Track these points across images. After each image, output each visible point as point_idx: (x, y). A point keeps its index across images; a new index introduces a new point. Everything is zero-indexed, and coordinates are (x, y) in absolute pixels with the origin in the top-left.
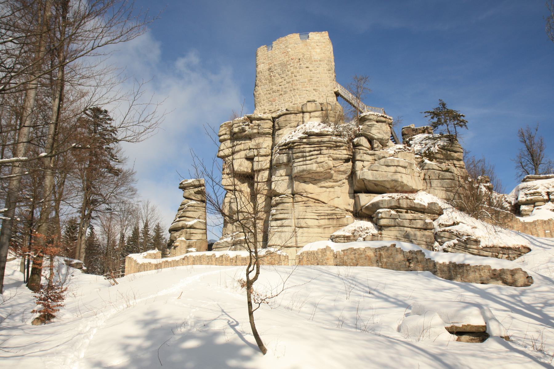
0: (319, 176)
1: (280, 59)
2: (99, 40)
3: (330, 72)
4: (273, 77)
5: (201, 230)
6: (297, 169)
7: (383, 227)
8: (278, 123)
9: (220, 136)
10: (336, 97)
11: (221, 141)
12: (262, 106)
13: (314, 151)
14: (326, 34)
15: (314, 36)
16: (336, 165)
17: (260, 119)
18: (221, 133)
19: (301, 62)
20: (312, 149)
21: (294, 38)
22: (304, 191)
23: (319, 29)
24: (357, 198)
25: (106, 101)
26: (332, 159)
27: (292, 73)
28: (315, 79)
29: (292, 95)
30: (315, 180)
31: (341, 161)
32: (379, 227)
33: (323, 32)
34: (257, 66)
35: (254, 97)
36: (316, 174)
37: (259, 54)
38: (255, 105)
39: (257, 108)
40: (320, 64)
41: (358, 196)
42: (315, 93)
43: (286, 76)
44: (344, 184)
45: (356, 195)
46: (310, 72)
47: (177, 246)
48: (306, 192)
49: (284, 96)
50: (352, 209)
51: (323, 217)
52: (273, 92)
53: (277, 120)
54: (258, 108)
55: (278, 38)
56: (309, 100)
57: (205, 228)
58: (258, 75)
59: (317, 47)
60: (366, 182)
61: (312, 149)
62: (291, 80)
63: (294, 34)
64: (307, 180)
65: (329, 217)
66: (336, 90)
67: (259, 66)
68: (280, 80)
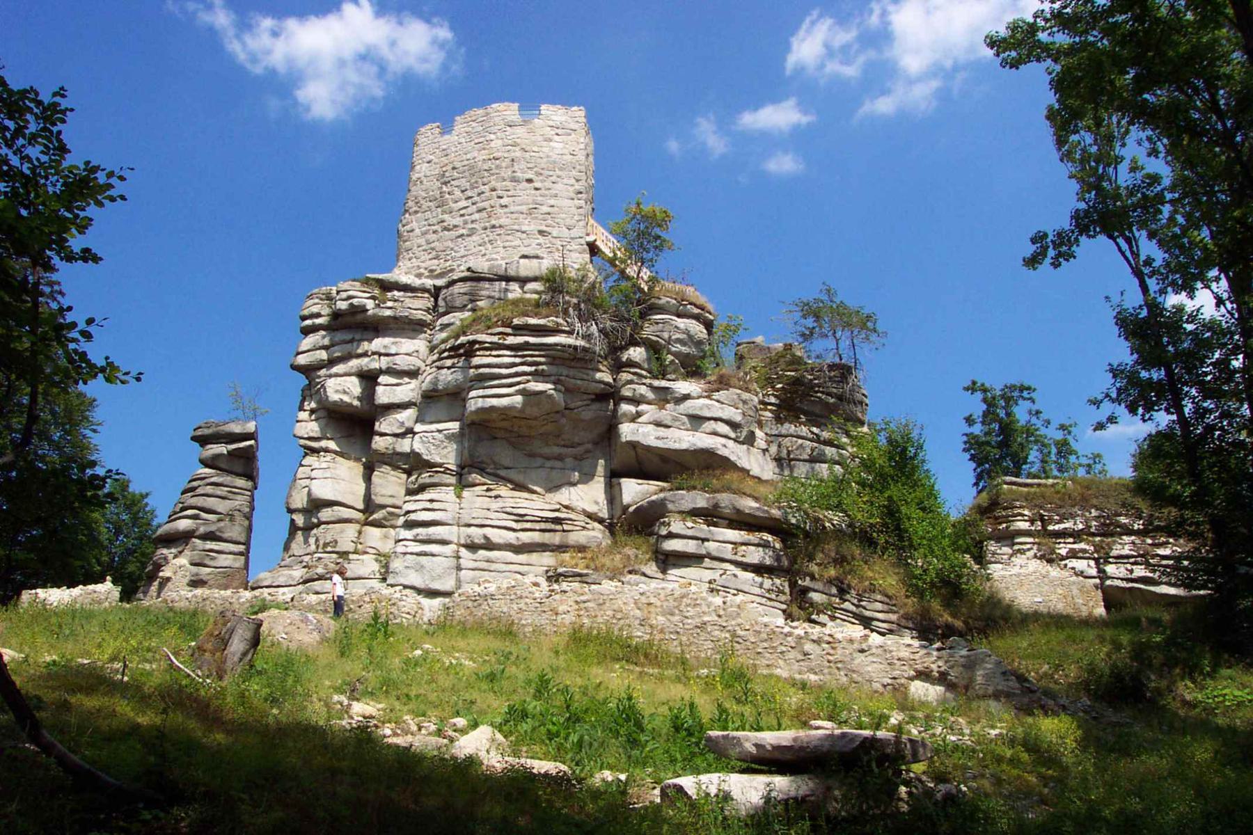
0: (530, 427)
1: (469, 156)
2: (398, 359)
3: (580, 196)
4: (447, 196)
5: (537, 533)
6: (476, 403)
7: (671, 558)
8: (444, 299)
9: (304, 318)
10: (591, 256)
11: (307, 331)
12: (414, 260)
13: (522, 364)
14: (579, 113)
15: (553, 114)
16: (572, 406)
17: (406, 288)
18: (306, 312)
19: (516, 167)
20: (518, 360)
21: (510, 110)
22: (489, 461)
23: (566, 101)
24: (616, 488)
25: (875, 665)
26: (563, 389)
27: (493, 190)
28: (545, 209)
29: (486, 239)
30: (519, 436)
31: (585, 397)
32: (661, 557)
33: (575, 108)
34: (413, 167)
35: (399, 237)
36: (523, 423)
37: (421, 140)
38: (398, 256)
39: (400, 264)
40: (558, 177)
41: (620, 484)
42: (541, 240)
43: (479, 194)
44: (588, 455)
45: (613, 480)
46: (534, 192)
47: (168, 579)
48: (494, 463)
49: (468, 239)
50: (604, 514)
51: (528, 525)
52: (445, 229)
53: (445, 291)
54: (404, 264)
55: (470, 109)
56: (526, 253)
57: (242, 539)
58: (412, 189)
59: (556, 138)
60: (639, 451)
61: (518, 360)
62: (486, 204)
63: (506, 104)
64: (500, 434)
65: (543, 526)
66: (590, 239)
67: (418, 167)
68: (463, 203)
